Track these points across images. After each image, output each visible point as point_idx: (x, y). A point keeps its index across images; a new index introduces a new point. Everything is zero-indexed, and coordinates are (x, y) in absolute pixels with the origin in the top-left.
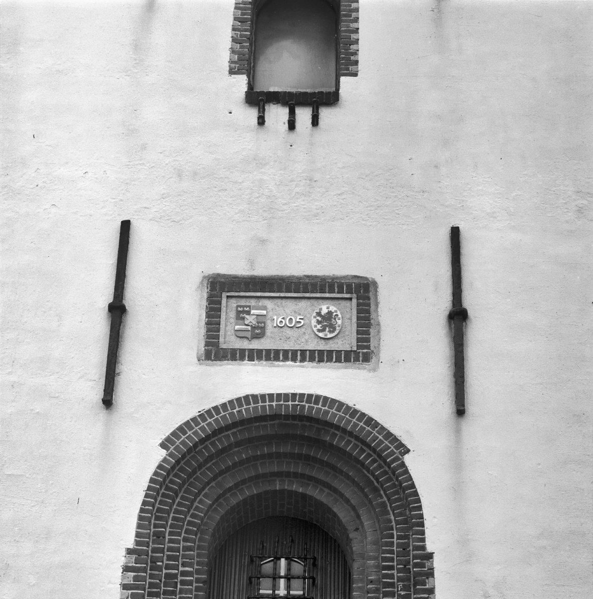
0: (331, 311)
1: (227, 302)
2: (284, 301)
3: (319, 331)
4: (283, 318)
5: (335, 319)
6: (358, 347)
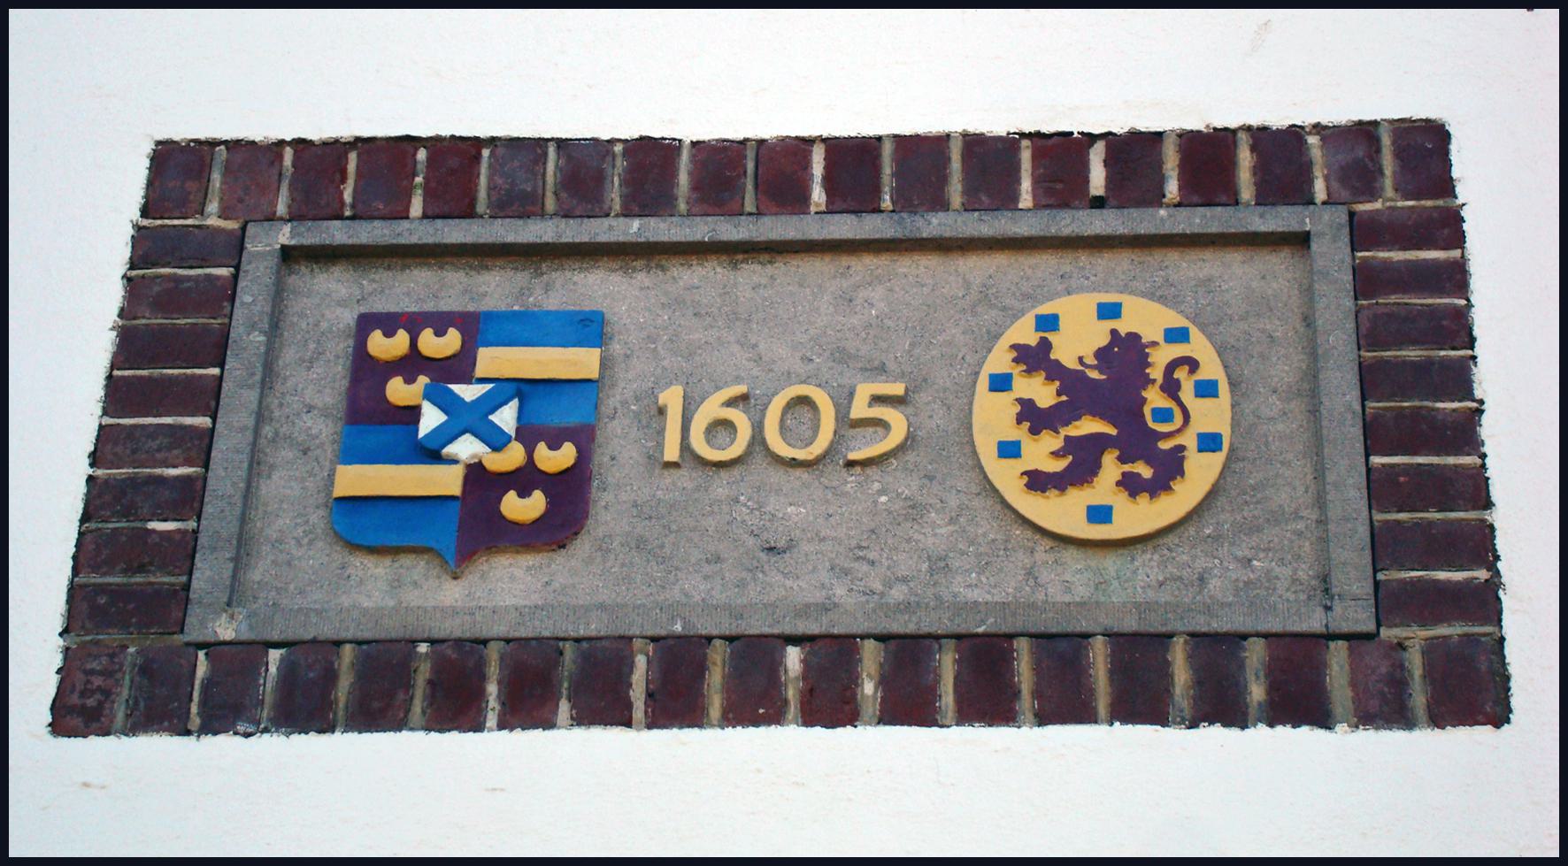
0: (1134, 337)
1: (279, 295)
2: (752, 274)
3: (1037, 482)
6: (1389, 603)
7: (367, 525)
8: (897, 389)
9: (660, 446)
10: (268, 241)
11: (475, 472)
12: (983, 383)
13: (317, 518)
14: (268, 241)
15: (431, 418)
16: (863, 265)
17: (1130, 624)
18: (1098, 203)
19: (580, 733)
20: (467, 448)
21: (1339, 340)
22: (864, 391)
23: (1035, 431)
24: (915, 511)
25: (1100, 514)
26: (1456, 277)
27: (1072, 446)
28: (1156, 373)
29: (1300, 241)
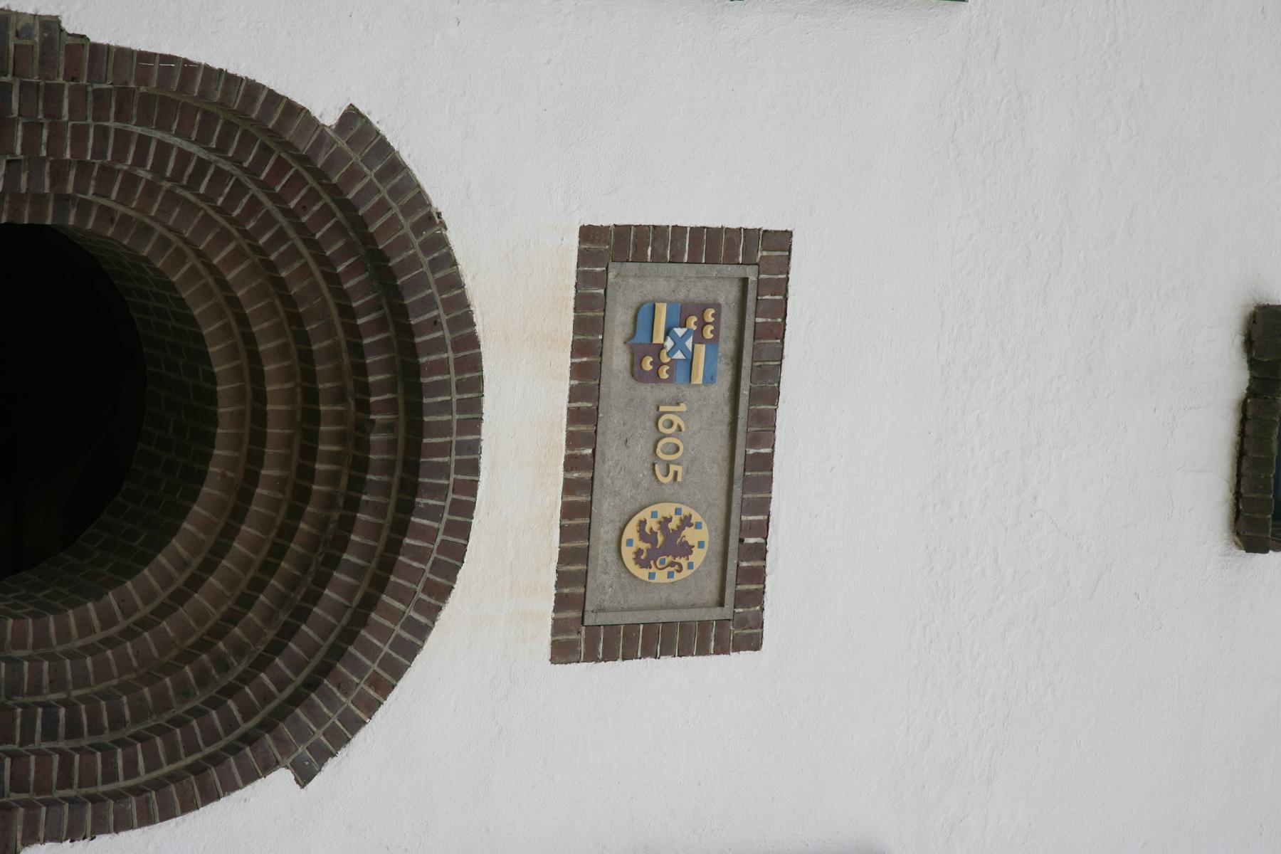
2: (724, 429)
3: (642, 524)
4: (679, 429)
5: (672, 564)
6: (593, 630)
7: (643, 314)
8: (679, 479)
9: (666, 404)
10: (751, 274)
11: (662, 347)
12: (678, 506)
13: (650, 297)
14: (751, 274)
15: (680, 332)
16: (725, 465)
17: (591, 553)
18: (741, 541)
19: (567, 388)
20: (669, 344)
21: (683, 616)
22: (680, 469)
23: (660, 523)
24: (636, 485)
25: (630, 543)
26: (703, 651)
27: (654, 534)
28: (677, 560)
29: (721, 604)
